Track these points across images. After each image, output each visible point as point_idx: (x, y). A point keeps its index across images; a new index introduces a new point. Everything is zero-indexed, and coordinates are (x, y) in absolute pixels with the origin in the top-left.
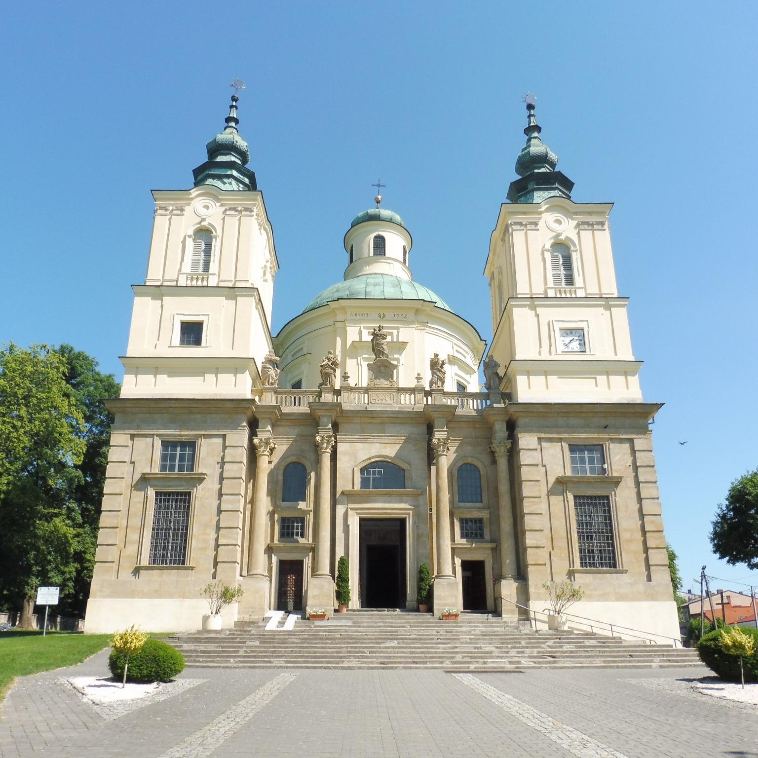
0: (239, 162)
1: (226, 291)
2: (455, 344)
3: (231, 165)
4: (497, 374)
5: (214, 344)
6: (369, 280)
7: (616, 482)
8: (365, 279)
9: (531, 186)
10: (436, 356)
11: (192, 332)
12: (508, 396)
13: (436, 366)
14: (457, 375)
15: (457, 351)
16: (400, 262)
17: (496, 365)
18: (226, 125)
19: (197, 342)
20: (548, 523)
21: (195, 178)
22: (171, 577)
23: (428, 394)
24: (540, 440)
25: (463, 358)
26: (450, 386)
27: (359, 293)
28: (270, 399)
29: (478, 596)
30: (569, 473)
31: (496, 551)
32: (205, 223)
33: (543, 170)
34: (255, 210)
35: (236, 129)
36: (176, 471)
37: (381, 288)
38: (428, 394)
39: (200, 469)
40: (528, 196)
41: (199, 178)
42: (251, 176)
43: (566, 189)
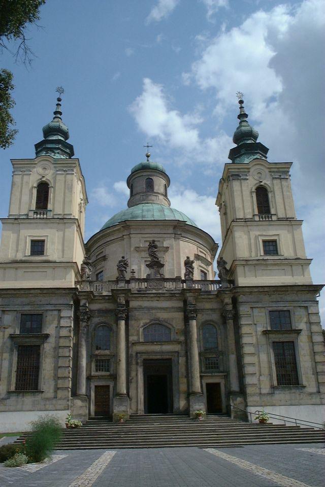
0: (62, 139)
1: (58, 221)
2: (199, 247)
3: (59, 142)
4: (225, 268)
5: (52, 252)
6: (144, 208)
7: (298, 332)
8: (141, 207)
9: (243, 151)
10: (188, 258)
11: (38, 247)
12: (232, 282)
13: (188, 264)
14: (200, 266)
15: (200, 251)
16: (162, 194)
17: (225, 263)
18: (54, 116)
20: (259, 363)
21: (36, 150)
22: (28, 399)
23: (183, 282)
24: (285, 425)
25: (203, 255)
26: (197, 276)
27: (137, 217)
28: (87, 288)
29: (215, 405)
30: (269, 329)
31: (227, 377)
32: (44, 179)
33: (249, 142)
34: (75, 170)
35: (60, 118)
36: (232, 418)
37: (150, 214)
38: (183, 282)
39: (46, 331)
40: (241, 158)
41: (39, 150)
42: (71, 147)
43: (264, 153)
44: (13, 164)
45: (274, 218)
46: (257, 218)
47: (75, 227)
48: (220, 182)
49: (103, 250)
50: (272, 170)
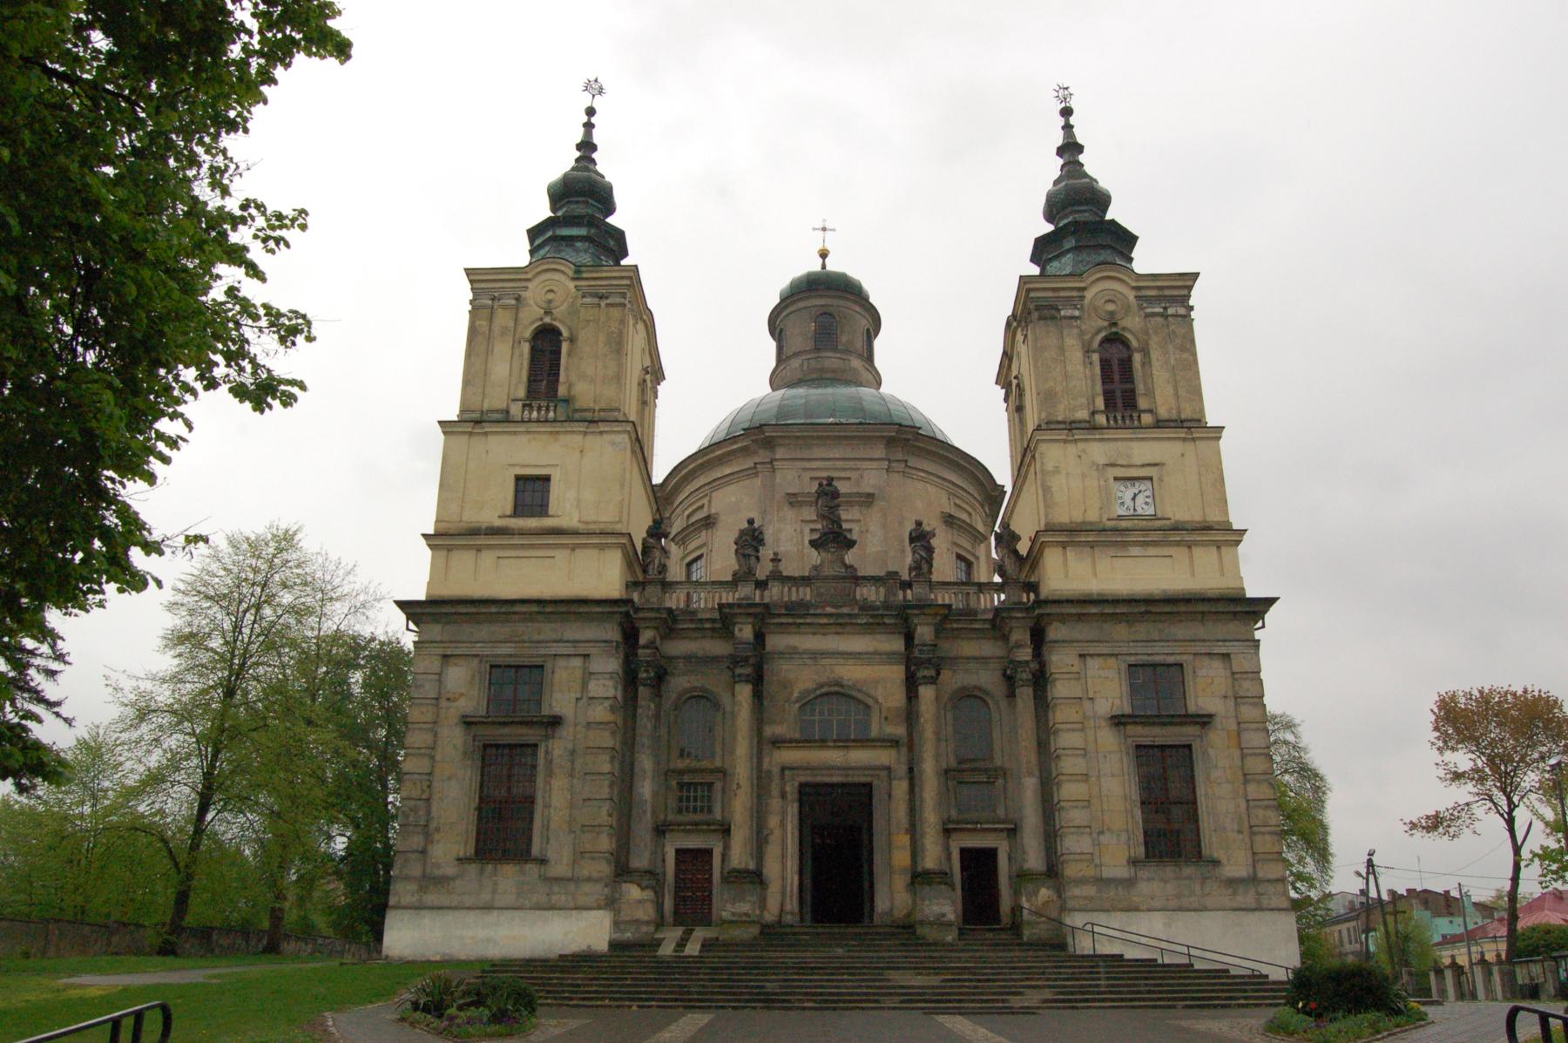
4: (1016, 552)
5: (566, 507)
11: (532, 491)
19: (542, 509)
21: (532, 241)
44: (471, 282)
45: (1147, 419)
46: (1101, 419)
47: (624, 440)
48: (1008, 324)
49: (705, 501)
50: (1145, 293)
